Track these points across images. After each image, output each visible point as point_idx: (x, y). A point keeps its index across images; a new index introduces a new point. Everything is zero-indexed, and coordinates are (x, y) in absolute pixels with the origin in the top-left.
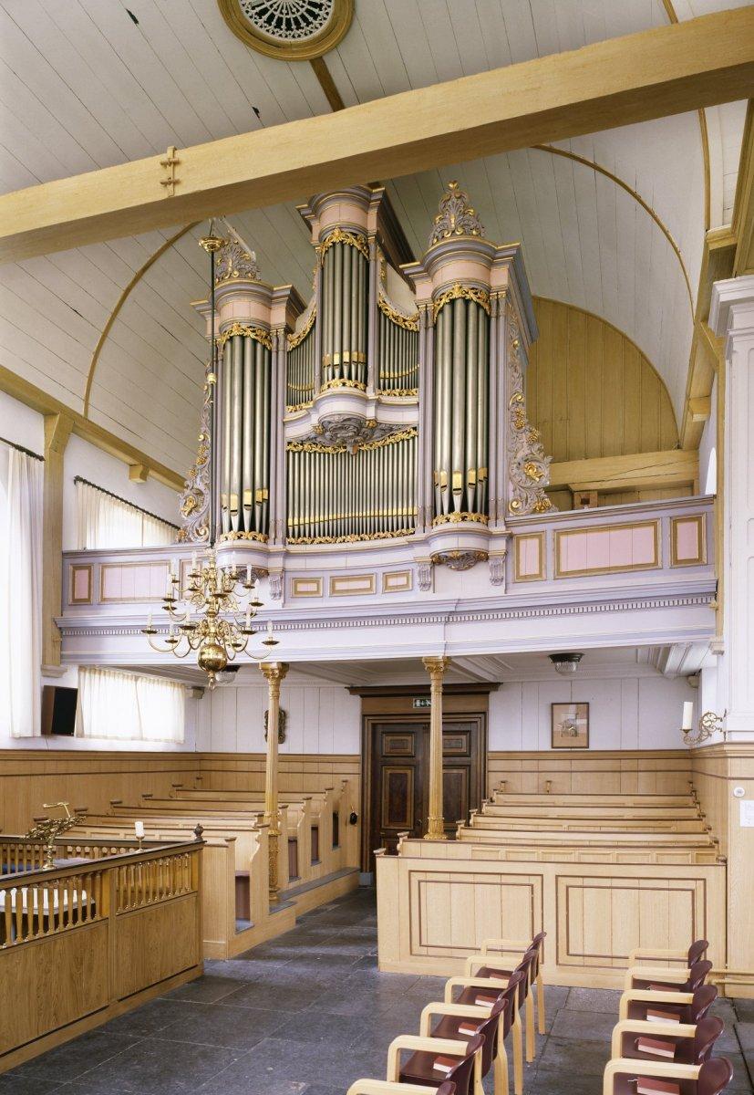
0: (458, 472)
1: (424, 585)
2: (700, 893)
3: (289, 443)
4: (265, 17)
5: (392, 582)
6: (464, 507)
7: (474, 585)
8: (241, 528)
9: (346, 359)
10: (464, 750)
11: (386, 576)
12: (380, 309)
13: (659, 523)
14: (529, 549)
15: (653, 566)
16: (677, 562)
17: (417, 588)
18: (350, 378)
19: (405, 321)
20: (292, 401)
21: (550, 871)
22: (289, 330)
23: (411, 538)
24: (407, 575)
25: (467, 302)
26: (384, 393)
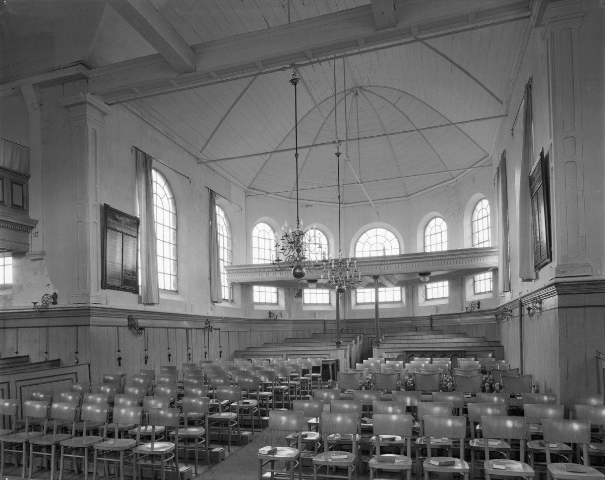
13: (5, 180)
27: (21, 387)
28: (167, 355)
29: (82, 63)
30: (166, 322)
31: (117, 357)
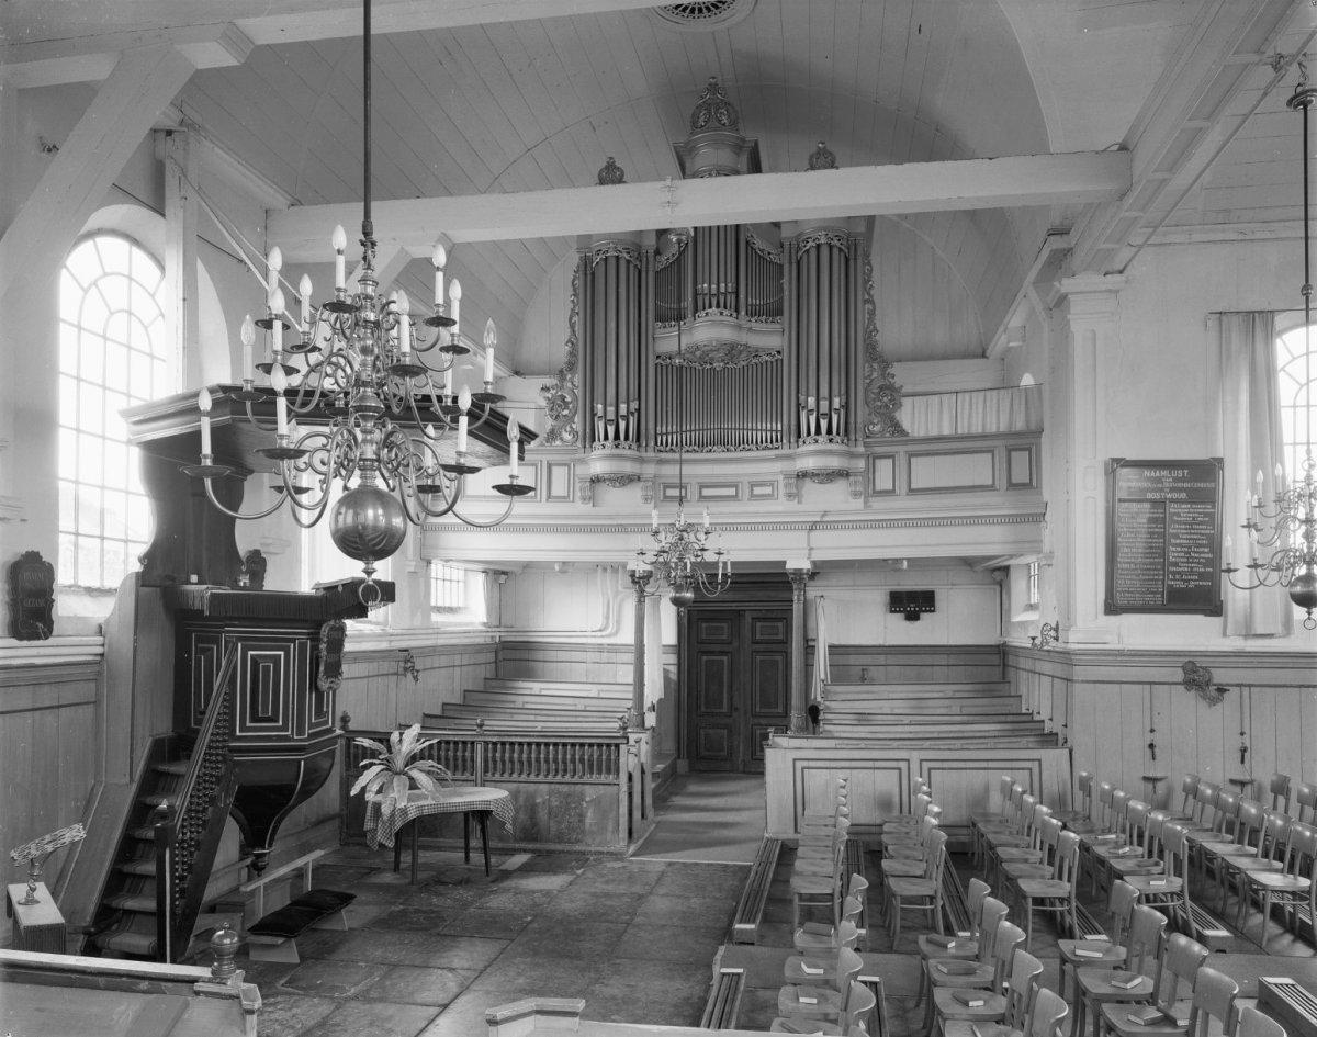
0: (825, 398)
1: (790, 496)
2: (805, 764)
3: (658, 357)
4: (696, 12)
5: (757, 491)
6: (829, 431)
7: (835, 498)
8: (617, 437)
9: (723, 290)
10: (780, 637)
11: (753, 485)
12: (747, 242)
13: (996, 452)
14: (884, 467)
15: (991, 488)
16: (1012, 486)
17: (782, 498)
18: (725, 308)
19: (769, 254)
20: (661, 317)
21: (915, 756)
22: (658, 252)
23: (777, 452)
24: (772, 485)
25: (831, 247)
26: (753, 320)
27: (899, 769)
28: (1147, 746)
29: (1053, 233)
30: (1153, 670)
31: (1149, 743)
